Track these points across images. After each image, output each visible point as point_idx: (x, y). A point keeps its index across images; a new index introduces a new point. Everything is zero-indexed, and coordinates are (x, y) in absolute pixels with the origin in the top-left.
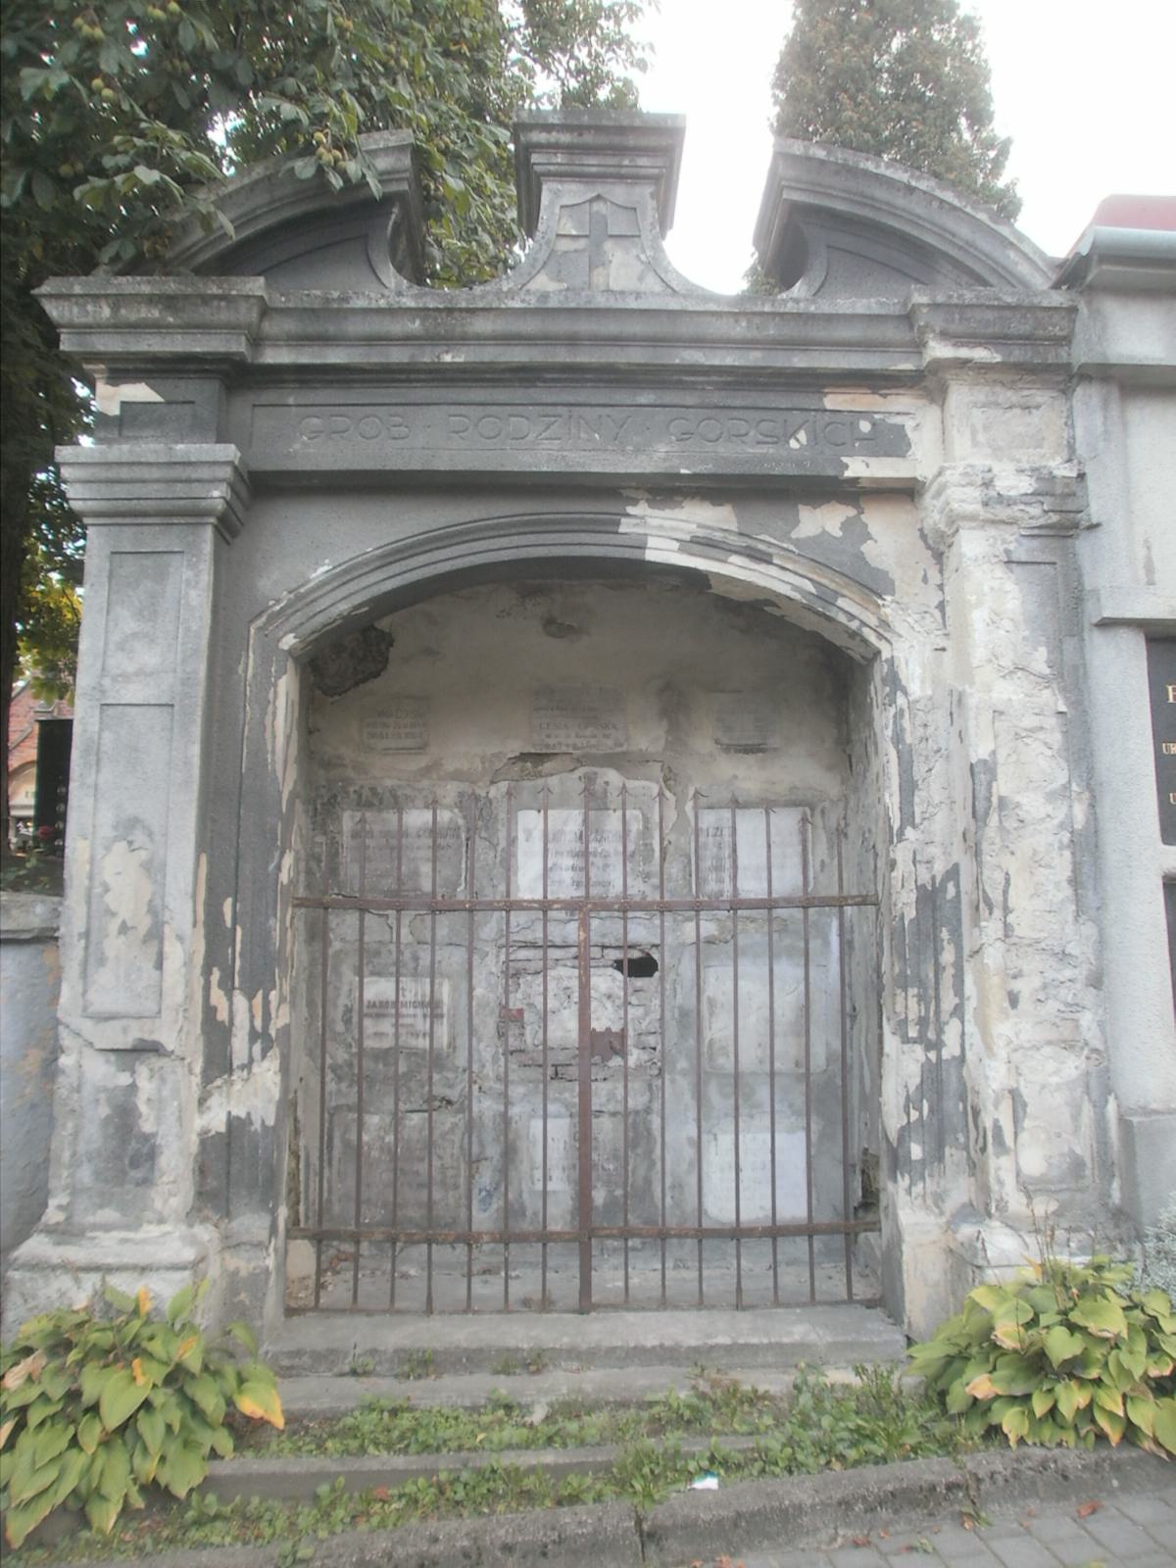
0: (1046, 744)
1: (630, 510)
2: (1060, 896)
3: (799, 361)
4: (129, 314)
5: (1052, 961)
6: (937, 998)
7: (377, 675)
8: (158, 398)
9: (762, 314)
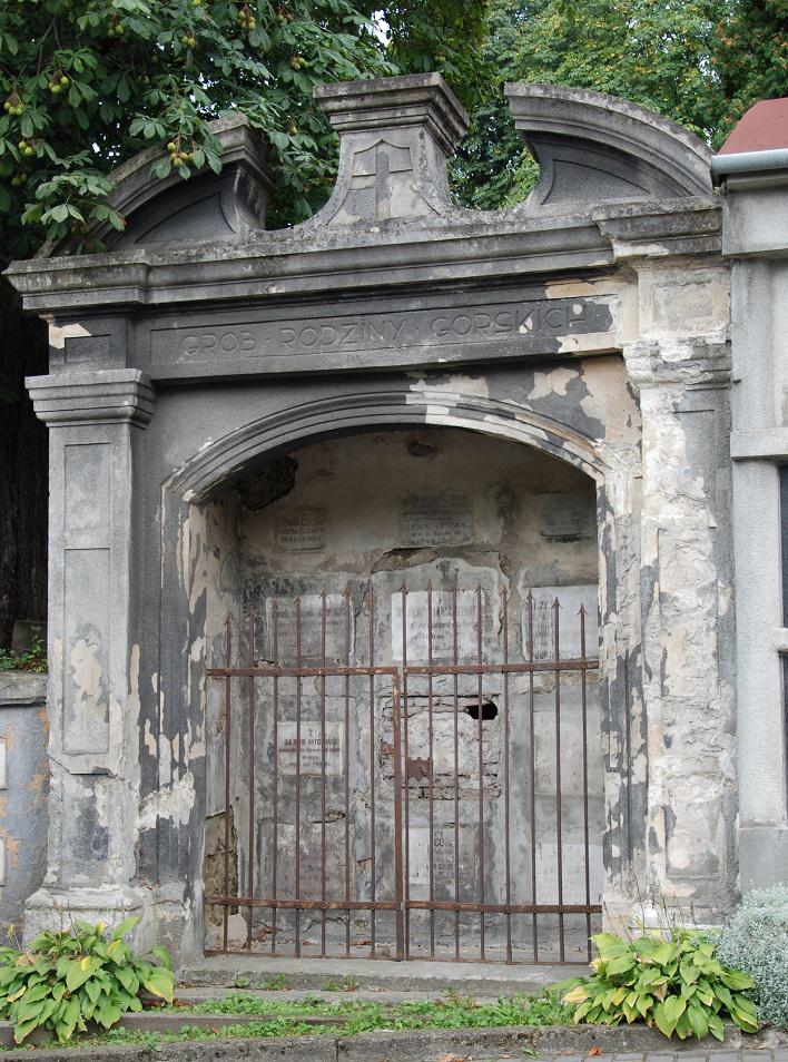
0: (700, 551)
1: (412, 388)
2: (706, 666)
3: (520, 267)
4: (63, 282)
5: (700, 714)
6: (628, 739)
7: (286, 492)
8: (86, 334)
9: (487, 237)
